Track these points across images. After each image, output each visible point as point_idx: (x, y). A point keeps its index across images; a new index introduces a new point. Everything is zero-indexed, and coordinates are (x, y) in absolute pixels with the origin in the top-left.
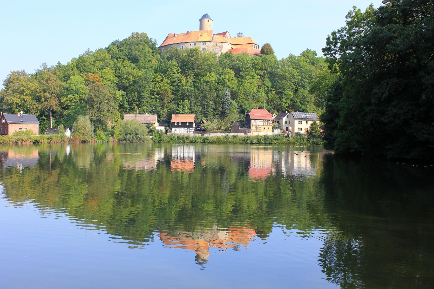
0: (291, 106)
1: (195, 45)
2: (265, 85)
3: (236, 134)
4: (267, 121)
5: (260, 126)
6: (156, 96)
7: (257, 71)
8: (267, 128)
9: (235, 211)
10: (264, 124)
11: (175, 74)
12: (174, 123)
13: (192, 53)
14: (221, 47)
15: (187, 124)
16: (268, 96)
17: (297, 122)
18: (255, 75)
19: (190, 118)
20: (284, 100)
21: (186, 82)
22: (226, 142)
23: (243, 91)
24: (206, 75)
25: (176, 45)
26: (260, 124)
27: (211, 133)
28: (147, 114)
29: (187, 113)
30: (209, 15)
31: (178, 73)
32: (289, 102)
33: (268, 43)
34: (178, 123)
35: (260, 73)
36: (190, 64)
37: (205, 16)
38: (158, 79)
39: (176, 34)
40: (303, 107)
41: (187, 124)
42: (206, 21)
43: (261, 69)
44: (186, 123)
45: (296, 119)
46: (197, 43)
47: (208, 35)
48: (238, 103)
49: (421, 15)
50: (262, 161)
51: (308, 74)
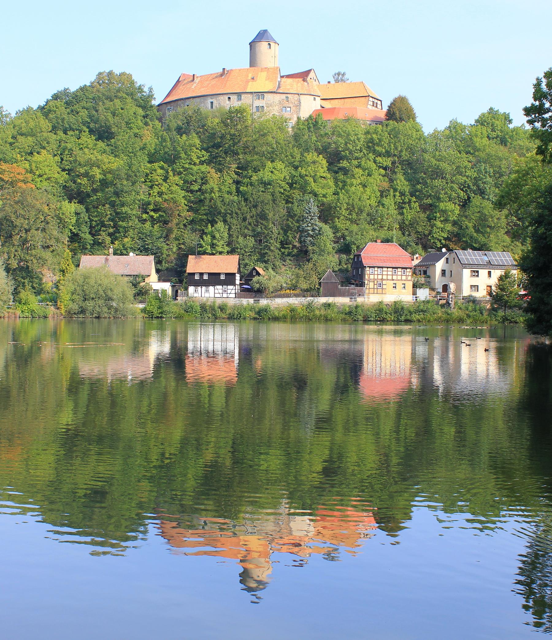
1: (240, 99)
2: (395, 190)
6: (152, 213)
7: (379, 159)
9: (327, 472)
11: (195, 164)
12: (193, 274)
13: (234, 117)
14: (298, 105)
15: (223, 277)
16: (402, 214)
17: (467, 272)
18: (374, 166)
19: (227, 264)
20: (439, 224)
21: (219, 184)
22: (309, 317)
23: (348, 204)
24: (264, 166)
25: (198, 100)
27: (276, 297)
28: (131, 254)
29: (221, 253)
30: (272, 33)
31: (202, 163)
32: (449, 227)
33: (403, 94)
34: (201, 274)
36: (227, 141)
37: (262, 35)
38: (158, 176)
39: (198, 74)
40: (481, 238)
41: (223, 277)
42: (263, 46)
43: (388, 154)
45: (465, 266)
46: (243, 96)
47: (268, 78)
48: (336, 230)
50: (389, 358)
51: (492, 166)
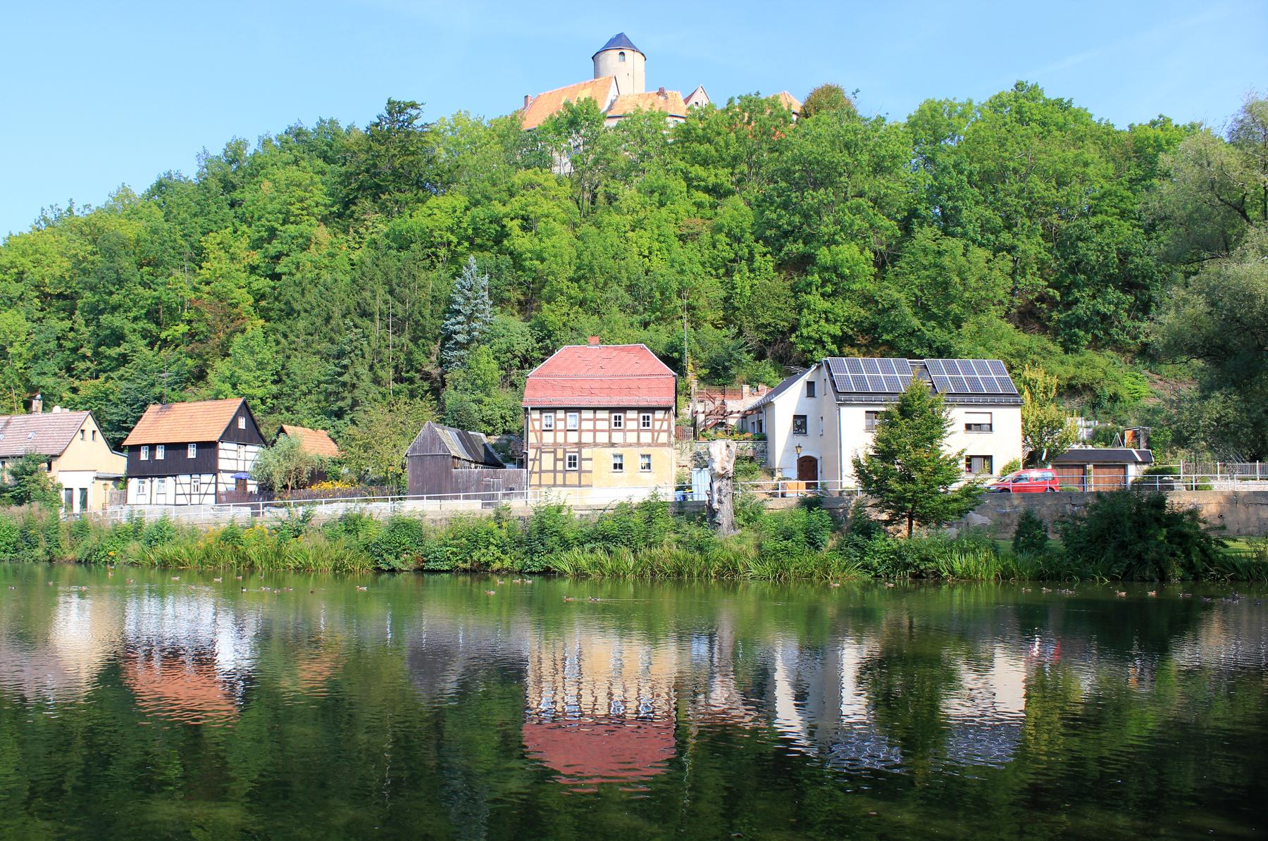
0: (864, 331)
3: (355, 507)
4: (587, 415)
5: (586, 453)
8: (633, 460)
10: (617, 437)
26: (588, 437)
34: (152, 447)
35: (712, 180)
41: (192, 453)
44: (184, 446)
49: (1166, 537)
